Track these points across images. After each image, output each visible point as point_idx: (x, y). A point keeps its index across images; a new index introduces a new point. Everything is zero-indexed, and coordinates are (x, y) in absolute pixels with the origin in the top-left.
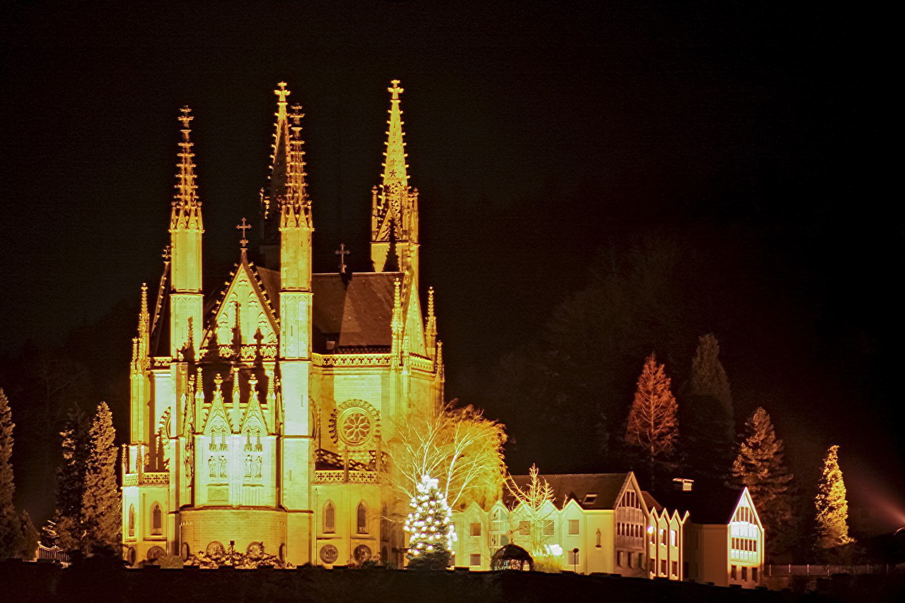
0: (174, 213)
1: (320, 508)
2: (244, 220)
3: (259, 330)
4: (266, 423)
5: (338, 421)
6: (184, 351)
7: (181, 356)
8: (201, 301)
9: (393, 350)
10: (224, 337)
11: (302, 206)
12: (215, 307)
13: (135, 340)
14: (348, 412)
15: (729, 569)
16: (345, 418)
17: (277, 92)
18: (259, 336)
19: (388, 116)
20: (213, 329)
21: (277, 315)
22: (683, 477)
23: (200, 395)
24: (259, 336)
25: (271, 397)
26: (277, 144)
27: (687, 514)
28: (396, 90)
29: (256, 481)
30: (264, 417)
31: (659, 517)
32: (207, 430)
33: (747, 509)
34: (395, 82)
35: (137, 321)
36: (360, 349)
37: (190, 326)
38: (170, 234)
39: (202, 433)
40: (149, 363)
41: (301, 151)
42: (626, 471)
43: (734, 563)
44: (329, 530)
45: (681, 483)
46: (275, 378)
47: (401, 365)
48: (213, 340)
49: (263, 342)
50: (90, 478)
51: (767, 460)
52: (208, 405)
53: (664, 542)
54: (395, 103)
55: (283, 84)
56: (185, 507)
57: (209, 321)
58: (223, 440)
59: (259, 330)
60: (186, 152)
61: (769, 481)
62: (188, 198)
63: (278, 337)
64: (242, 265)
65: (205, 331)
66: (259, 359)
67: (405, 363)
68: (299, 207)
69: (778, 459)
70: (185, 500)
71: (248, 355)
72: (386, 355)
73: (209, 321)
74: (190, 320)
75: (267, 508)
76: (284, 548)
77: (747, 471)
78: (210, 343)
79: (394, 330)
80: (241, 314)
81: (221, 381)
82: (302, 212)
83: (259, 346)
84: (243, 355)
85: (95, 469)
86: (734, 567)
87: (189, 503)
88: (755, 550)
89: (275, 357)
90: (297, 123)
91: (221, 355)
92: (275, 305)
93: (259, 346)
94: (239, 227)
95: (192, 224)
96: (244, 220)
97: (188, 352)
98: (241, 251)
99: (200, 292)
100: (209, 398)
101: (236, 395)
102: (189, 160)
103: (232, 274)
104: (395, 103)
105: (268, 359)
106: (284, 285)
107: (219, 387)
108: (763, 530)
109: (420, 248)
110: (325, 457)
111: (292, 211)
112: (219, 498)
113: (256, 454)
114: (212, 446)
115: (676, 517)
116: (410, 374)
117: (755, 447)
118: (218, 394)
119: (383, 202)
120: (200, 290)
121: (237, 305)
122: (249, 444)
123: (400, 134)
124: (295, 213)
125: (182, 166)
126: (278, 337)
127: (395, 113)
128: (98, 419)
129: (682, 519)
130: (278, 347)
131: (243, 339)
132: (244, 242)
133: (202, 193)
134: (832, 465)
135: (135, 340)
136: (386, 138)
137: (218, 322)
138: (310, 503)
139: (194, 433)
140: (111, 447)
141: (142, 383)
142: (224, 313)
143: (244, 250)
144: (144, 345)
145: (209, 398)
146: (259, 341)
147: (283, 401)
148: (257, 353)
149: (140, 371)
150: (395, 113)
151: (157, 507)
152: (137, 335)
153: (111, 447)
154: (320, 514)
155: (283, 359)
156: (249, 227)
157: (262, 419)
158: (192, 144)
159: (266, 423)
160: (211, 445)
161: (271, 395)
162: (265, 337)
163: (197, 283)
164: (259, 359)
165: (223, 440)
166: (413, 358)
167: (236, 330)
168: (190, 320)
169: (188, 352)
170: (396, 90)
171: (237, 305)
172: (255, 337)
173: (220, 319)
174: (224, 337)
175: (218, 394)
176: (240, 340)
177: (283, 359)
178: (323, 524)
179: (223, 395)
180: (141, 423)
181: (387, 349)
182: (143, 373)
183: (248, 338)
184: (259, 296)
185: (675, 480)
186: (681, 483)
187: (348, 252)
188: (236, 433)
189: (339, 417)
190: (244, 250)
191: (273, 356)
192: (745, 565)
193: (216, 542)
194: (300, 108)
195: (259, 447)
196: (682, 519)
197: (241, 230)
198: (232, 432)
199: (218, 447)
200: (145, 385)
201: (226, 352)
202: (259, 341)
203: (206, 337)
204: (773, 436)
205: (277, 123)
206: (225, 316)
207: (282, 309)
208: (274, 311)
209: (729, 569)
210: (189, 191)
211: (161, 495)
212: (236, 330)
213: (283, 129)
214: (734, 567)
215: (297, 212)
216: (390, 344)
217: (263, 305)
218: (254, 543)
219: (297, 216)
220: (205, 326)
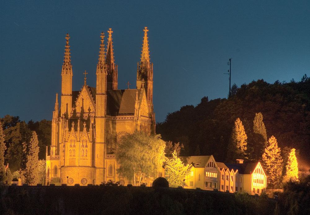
0: (63, 69)
1: (108, 167)
2: (86, 71)
3: (89, 107)
4: (89, 138)
5: (117, 139)
6: (65, 115)
7: (64, 117)
8: (71, 98)
9: (135, 115)
10: (78, 110)
11: (103, 66)
12: (76, 100)
13: (54, 112)
14: (120, 136)
15: (252, 189)
16: (120, 138)
17: (108, 32)
18: (89, 110)
19: (143, 39)
20: (75, 107)
21: (95, 103)
22: (239, 159)
23: (67, 129)
24: (89, 110)
25: (91, 129)
26: (108, 49)
27: (237, 171)
28: (146, 31)
29: (85, 158)
30: (88, 136)
31: (230, 172)
32: (69, 140)
33: (259, 169)
34: (146, 28)
35: (54, 105)
36: (125, 114)
37: (67, 106)
38: (62, 76)
39: (67, 142)
40: (58, 120)
41: (103, 48)
42: (236, 161)
43: (254, 188)
44: (111, 175)
45: (239, 161)
46: (95, 124)
47: (138, 119)
48: (75, 111)
49: (91, 111)
50: (29, 157)
51: (274, 155)
52: (70, 132)
53: (227, 179)
54: (146, 35)
55: (110, 29)
56: (62, 166)
57: (74, 105)
58: (74, 144)
59: (89, 107)
60: (67, 49)
61: (275, 162)
62: (67, 64)
63: (95, 110)
64: (84, 86)
65: (73, 108)
66: (89, 117)
67: (139, 119)
68: (102, 67)
69: (279, 154)
70: (62, 165)
71: (86, 116)
72: (133, 116)
73: (74, 105)
74: (67, 104)
75: (88, 167)
76: (95, 181)
77: (267, 158)
78: (74, 112)
79: (136, 108)
80: (84, 102)
81: (74, 124)
82: (103, 68)
83: (89, 113)
84: (84, 116)
85: (31, 154)
86: (254, 189)
87: (63, 165)
88: (263, 183)
89: (94, 116)
90: (103, 39)
91: (77, 116)
92: (94, 99)
93: (89, 113)
94: (84, 74)
95: (69, 73)
96: (86, 71)
97: (66, 115)
98: (84, 82)
99: (71, 95)
100: (70, 130)
101: (79, 129)
102: (68, 51)
103: (81, 89)
104: (146, 35)
105: (92, 117)
106: (97, 92)
107: (73, 126)
108: (266, 177)
109: (153, 83)
110: (113, 151)
111: (100, 68)
112: (72, 163)
113: (85, 149)
114: (71, 146)
115: (228, 171)
116: (141, 122)
117: (271, 150)
118: (73, 129)
119: (141, 67)
120: (71, 94)
121: (83, 99)
122: (83, 146)
123: (147, 45)
124: (101, 68)
125: (66, 53)
126: (95, 110)
127: (146, 38)
128: (32, 137)
129: (235, 172)
130: (95, 113)
131: (84, 111)
132: (85, 79)
133: (72, 63)
134: (293, 156)
135: (54, 112)
136: (142, 46)
137: (77, 105)
138: (104, 165)
139: (65, 142)
140: (37, 146)
141: (55, 126)
142: (141, 116)
143: (85, 81)
144: (56, 113)
145: (70, 130)
146: (89, 111)
147: (96, 131)
148: (89, 115)
149: (54, 122)
150: (146, 38)
151: (56, 167)
152: (55, 110)
153: (37, 146)
154: (108, 169)
155: (96, 117)
156: (84, 74)
157: (87, 137)
158: (69, 46)
159: (89, 138)
160: (70, 146)
161: (91, 129)
162: (91, 110)
163: (70, 92)
164: (89, 117)
165: (74, 144)
166: (142, 117)
167: (82, 108)
168: (67, 104)
169: (66, 115)
170: (146, 31)
171: (82, 99)
172: (88, 110)
173: (77, 104)
174: (78, 110)
175: (73, 129)
176: (84, 111)
177: (96, 117)
178: (109, 173)
179: (74, 129)
180: (54, 140)
181: (133, 114)
182: (55, 123)
183: (86, 110)
184: (90, 96)
185: (237, 160)
186: (239, 161)
187: (87, 73)
188: (78, 141)
189: (118, 137)
190: (85, 81)
191: (93, 116)
192: (258, 188)
193: (71, 178)
194: (104, 34)
195: (87, 146)
196: (235, 172)
197: (85, 74)
198: (77, 141)
199: (73, 146)
200: (56, 127)
201: (78, 115)
202: (89, 111)
203: (72, 110)
204: (277, 147)
205: (108, 42)
206: (79, 102)
207: (96, 100)
208: (94, 101)
209: (252, 189)
210: (68, 62)
211: (56, 163)
212: (82, 108)
213: (110, 44)
214: (254, 189)
215: (101, 68)
216: (133, 113)
217: (91, 99)
218: (84, 179)
219: (102, 69)
220: (72, 107)
